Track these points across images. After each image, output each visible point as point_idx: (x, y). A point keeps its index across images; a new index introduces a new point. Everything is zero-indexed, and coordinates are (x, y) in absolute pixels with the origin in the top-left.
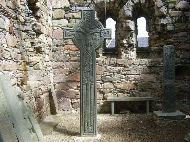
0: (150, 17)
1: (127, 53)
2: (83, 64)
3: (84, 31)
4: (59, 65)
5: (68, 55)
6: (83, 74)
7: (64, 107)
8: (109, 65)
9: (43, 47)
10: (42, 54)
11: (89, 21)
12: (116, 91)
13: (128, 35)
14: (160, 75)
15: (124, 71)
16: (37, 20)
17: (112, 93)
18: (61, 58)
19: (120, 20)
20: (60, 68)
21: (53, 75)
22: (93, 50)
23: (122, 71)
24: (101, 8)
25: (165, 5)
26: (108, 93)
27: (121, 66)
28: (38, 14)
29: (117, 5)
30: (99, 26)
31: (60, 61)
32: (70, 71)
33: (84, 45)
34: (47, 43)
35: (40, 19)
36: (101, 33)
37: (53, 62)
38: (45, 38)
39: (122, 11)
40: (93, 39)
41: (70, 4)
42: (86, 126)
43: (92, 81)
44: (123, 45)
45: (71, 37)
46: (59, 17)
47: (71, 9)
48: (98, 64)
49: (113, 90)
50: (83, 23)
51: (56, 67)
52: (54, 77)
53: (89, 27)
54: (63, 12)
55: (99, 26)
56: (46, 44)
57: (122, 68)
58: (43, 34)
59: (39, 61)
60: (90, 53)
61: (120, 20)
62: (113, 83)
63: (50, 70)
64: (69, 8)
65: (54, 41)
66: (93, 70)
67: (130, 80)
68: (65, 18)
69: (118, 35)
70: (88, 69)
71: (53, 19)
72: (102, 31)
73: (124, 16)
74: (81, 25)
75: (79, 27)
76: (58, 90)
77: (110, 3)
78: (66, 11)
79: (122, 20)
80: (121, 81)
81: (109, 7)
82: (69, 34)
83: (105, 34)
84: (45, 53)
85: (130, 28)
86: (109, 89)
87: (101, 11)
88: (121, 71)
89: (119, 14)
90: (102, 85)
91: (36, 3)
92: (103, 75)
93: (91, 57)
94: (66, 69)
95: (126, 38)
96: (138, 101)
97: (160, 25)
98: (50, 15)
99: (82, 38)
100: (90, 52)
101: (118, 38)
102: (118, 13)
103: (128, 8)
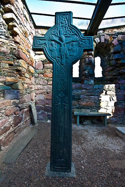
0: (105, 55)
3: (58, 39)
10: (22, 76)
21: (35, 94)
25: (120, 43)
32: (47, 92)
33: (58, 57)
36: (80, 42)
40: (69, 50)
43: (67, 102)
52: (35, 96)
57: (85, 90)
62: (78, 101)
70: (62, 87)
75: (52, 34)
83: (84, 43)
93: (66, 72)
96: (95, 116)
97: (115, 60)
100: (65, 66)
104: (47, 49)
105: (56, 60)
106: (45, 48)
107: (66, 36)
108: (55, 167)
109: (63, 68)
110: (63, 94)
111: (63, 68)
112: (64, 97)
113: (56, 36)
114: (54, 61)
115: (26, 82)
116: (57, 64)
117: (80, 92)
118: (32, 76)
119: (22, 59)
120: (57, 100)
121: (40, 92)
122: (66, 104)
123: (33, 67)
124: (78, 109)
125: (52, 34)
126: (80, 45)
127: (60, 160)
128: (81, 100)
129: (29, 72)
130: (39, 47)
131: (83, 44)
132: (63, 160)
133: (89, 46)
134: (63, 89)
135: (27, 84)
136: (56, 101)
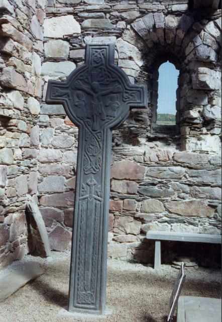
1: (199, 139)
2: (83, 156)
3: (88, 88)
6: (82, 178)
9: (14, 117)
11: (101, 69)
13: (203, 99)
15: (188, 177)
16: (4, 59)
17: (159, 222)
19: (187, 67)
21: (38, 175)
22: (105, 130)
23: (185, 176)
24: (147, 40)
26: (151, 221)
27: (181, 166)
29: (181, 34)
30: (120, 78)
33: (88, 118)
35: (10, 59)
36: (125, 95)
37: (40, 148)
38: (22, 99)
39: (193, 48)
41: (82, 29)
42: (82, 288)
43: (99, 193)
44: (190, 122)
45: (60, 101)
47: (84, 41)
48: (134, 159)
49: (162, 216)
50: (87, 72)
53: (99, 82)
57: (184, 169)
58: (16, 90)
60: (98, 134)
61: (187, 67)
62: (162, 201)
63: (31, 165)
64: (80, 38)
66: (104, 170)
67: (201, 198)
68: (70, 59)
69: (182, 101)
71: (46, 59)
72: (126, 89)
73: (195, 59)
74: (82, 76)
76: (47, 207)
77: (166, 31)
78: (73, 44)
79: (191, 66)
80: (180, 197)
81: (165, 40)
82: (57, 94)
85: (207, 86)
87: (148, 48)
88: (182, 176)
89: (187, 52)
90: (140, 203)
92: (142, 183)
95: (199, 106)
98: (37, 51)
100: (98, 133)
101: (182, 106)
102: (184, 53)
103: (206, 41)
104: (69, 104)
105: (84, 121)
107: (102, 82)
109: (96, 136)
116: (85, 130)
118: (35, 124)
119: (14, 89)
120: (83, 190)
121: (54, 169)
125: (79, 79)
126: (125, 100)
129: (28, 114)
131: (129, 98)
133: (139, 101)
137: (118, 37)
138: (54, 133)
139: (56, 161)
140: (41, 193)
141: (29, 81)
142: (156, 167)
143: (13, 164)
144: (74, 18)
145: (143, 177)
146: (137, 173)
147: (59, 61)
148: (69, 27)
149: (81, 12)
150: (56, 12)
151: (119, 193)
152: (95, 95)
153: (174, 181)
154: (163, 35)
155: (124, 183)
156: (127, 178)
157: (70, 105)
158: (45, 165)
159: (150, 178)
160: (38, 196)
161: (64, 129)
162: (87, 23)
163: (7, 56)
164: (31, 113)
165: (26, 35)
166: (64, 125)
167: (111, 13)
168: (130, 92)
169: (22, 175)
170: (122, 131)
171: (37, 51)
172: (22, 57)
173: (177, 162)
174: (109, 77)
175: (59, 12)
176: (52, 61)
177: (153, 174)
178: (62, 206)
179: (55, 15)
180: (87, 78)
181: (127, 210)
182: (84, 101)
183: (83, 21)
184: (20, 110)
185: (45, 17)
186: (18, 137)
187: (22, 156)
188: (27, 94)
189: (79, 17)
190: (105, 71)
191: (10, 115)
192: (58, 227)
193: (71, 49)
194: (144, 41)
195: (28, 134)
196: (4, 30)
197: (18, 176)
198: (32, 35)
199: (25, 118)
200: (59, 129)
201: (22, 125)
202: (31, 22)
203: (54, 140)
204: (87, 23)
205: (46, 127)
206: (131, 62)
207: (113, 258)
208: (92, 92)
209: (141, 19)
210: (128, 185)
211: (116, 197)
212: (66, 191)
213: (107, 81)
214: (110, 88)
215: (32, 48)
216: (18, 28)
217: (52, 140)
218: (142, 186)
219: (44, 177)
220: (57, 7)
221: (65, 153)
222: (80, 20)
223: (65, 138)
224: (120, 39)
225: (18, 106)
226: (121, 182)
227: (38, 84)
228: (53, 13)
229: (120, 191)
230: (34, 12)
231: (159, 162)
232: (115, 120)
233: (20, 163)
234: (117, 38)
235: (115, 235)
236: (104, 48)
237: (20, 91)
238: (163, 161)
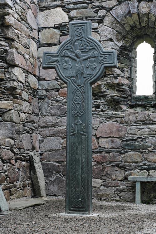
4: (50, 122)
5: (65, 106)
7: (56, 190)
8: (135, 123)
10: (17, 98)
11: (81, 40)
12: (146, 167)
14: (18, 33)
17: (139, 170)
18: (54, 111)
20: (50, 127)
21: (40, 138)
26: (132, 170)
28: (10, 34)
30: (96, 47)
31: (52, 115)
34: (27, 84)
46: (50, 42)
51: (44, 124)
52: (41, 142)
53: (80, 50)
54: (56, 34)
55: (96, 47)
56: (24, 85)
59: (10, 108)
60: (82, 88)
62: (141, 153)
63: (34, 128)
65: (41, 82)
70: (78, 112)
72: (101, 54)
76: (47, 162)
78: (63, 31)
84: (22, 98)
86: (135, 163)
87: (126, 31)
91: (6, 17)
94: (61, 128)
98: (33, 38)
99: (70, 67)
100: (82, 87)
104: (59, 67)
105: (71, 80)
106: (57, 65)
107: (83, 50)
108: (71, 208)
109: (80, 89)
110: (80, 121)
111: (80, 89)
112: (81, 124)
113: (71, 51)
114: (68, 81)
115: (24, 109)
117: (145, 132)
118: (35, 96)
120: (72, 128)
121: (52, 132)
122: (84, 132)
123: (34, 75)
124: (141, 170)
127: (77, 200)
128: (150, 149)
130: (53, 66)
132: (80, 200)
134: (80, 114)
135: (25, 113)
136: (72, 129)
137: (99, 23)
138: (51, 104)
139: (54, 126)
140: (42, 151)
141: (28, 61)
142: (135, 126)
143: (19, 124)
144: (63, 10)
145: (125, 135)
146: (119, 131)
147: (52, 46)
148: (59, 17)
149: (68, 4)
150: (47, 6)
151: (105, 148)
152: (77, 59)
153: (151, 137)
154: (138, 19)
155: (109, 141)
156: (112, 136)
157: (60, 69)
158: (44, 129)
159: (131, 135)
160: (40, 154)
161: (59, 100)
162: (73, 13)
163: (10, 40)
164: (31, 87)
165: (24, 25)
166: (58, 97)
167: (93, 4)
168: (104, 56)
169: (27, 134)
170: (106, 100)
171: (33, 38)
172: (22, 42)
173: (153, 121)
174: (88, 46)
175: (49, 6)
176: (46, 46)
177: (133, 132)
178: (60, 160)
179: (46, 8)
180: (72, 48)
181: (113, 161)
182: (70, 64)
183: (69, 12)
184: (23, 84)
185: (30, 197)
186: (22, 104)
187: (26, 119)
188: (27, 71)
189: (66, 8)
190: (84, 42)
191: (15, 86)
192: (57, 177)
193: (61, 36)
194: (122, 25)
195: (30, 103)
196: (7, 21)
197: (24, 134)
198: (29, 25)
199: (27, 90)
200: (54, 100)
201: (25, 95)
202: (27, 14)
203: (51, 109)
204: (73, 13)
205: (44, 99)
206: (111, 43)
207: (103, 199)
208: (76, 58)
209: (118, 7)
210: (112, 142)
211: (103, 152)
212: (62, 149)
213: (87, 49)
214: (90, 54)
215: (29, 36)
216: (18, 19)
217: (49, 109)
218: (124, 142)
219: (44, 138)
220: (48, 2)
221: (60, 119)
222: (68, 11)
223: (60, 107)
224: (101, 25)
225: (21, 79)
226: (106, 140)
227: (36, 65)
228: (44, 7)
229: (106, 147)
230: (29, 7)
231: (137, 122)
232: (93, 77)
233: (25, 124)
234: (99, 24)
235: (104, 182)
236: (83, 25)
237: (21, 68)
238: (140, 121)
